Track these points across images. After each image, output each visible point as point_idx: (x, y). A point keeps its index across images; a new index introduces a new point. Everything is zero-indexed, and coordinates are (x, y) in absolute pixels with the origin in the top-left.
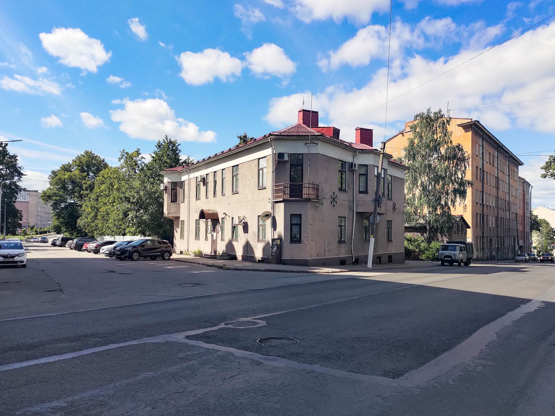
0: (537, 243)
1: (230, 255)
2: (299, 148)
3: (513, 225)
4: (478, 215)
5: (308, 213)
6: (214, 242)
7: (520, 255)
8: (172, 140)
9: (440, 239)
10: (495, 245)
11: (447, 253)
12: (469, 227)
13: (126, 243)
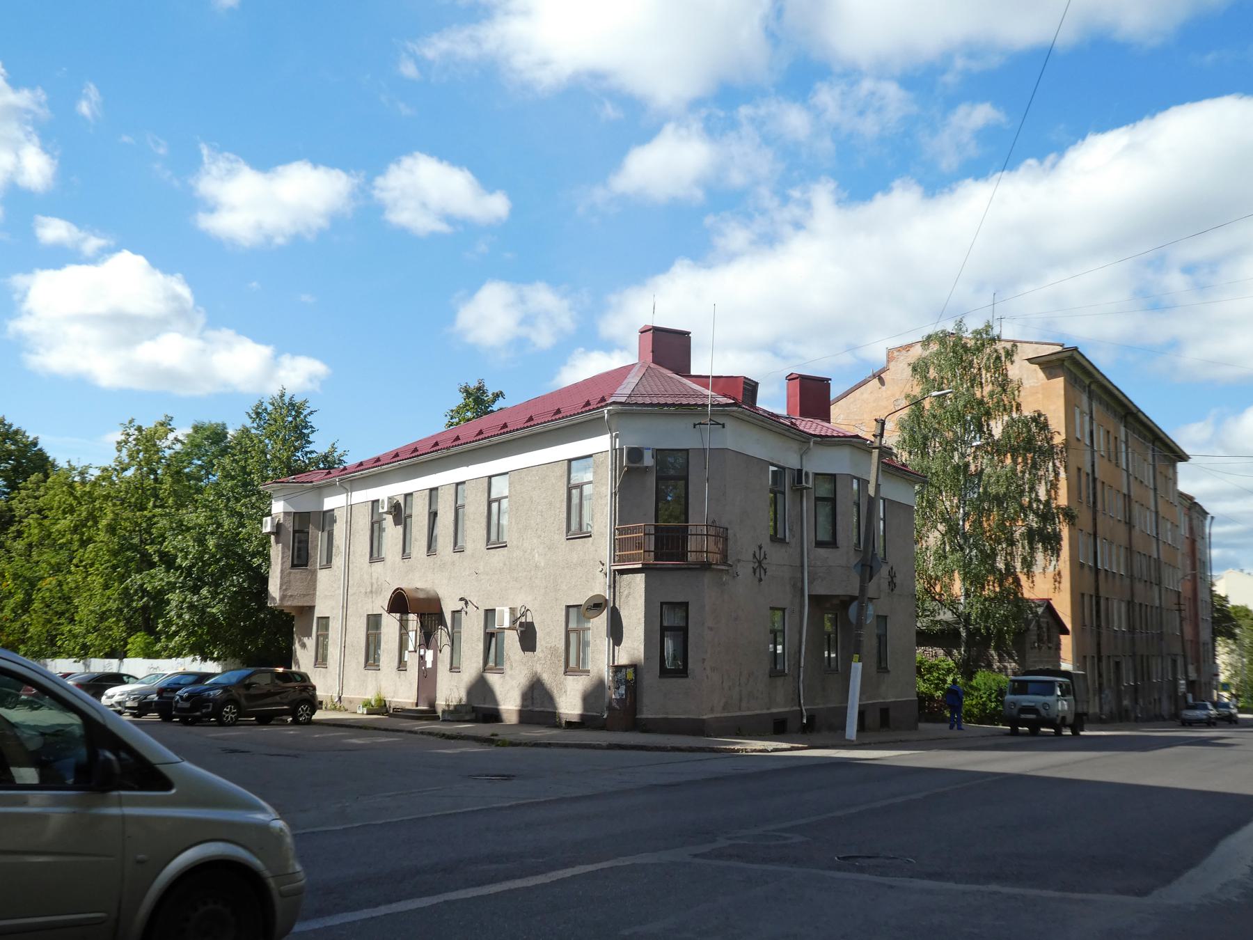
0: (1227, 673)
1: (480, 706)
2: (678, 435)
4: (1087, 599)
5: (708, 603)
6: (427, 678)
7: (1194, 707)
8: (298, 400)
9: (996, 665)
10: (1128, 681)
11: (1026, 700)
12: (1066, 632)
13: (191, 679)
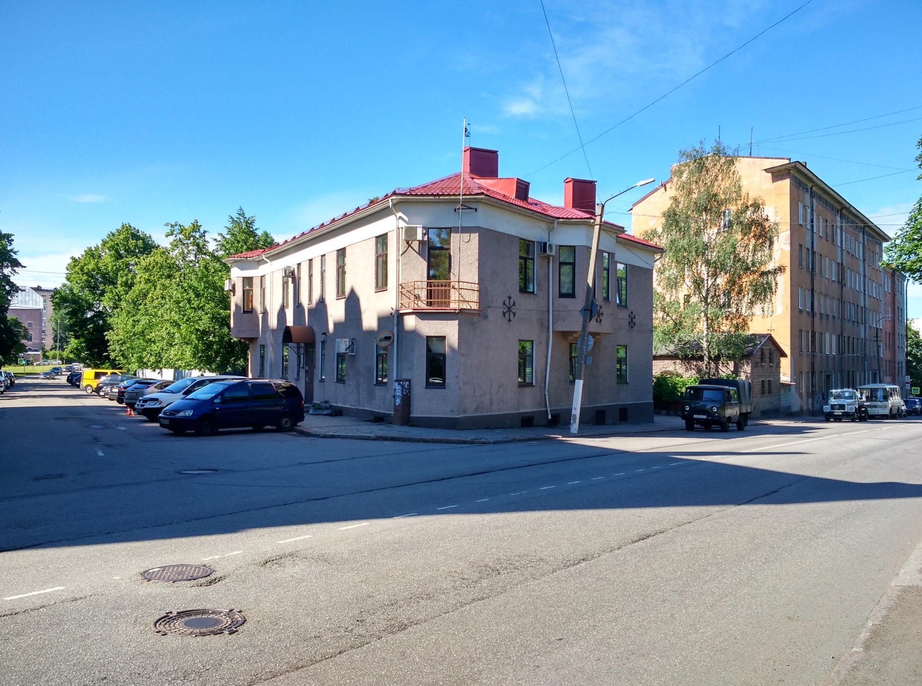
3: (871, 349)
